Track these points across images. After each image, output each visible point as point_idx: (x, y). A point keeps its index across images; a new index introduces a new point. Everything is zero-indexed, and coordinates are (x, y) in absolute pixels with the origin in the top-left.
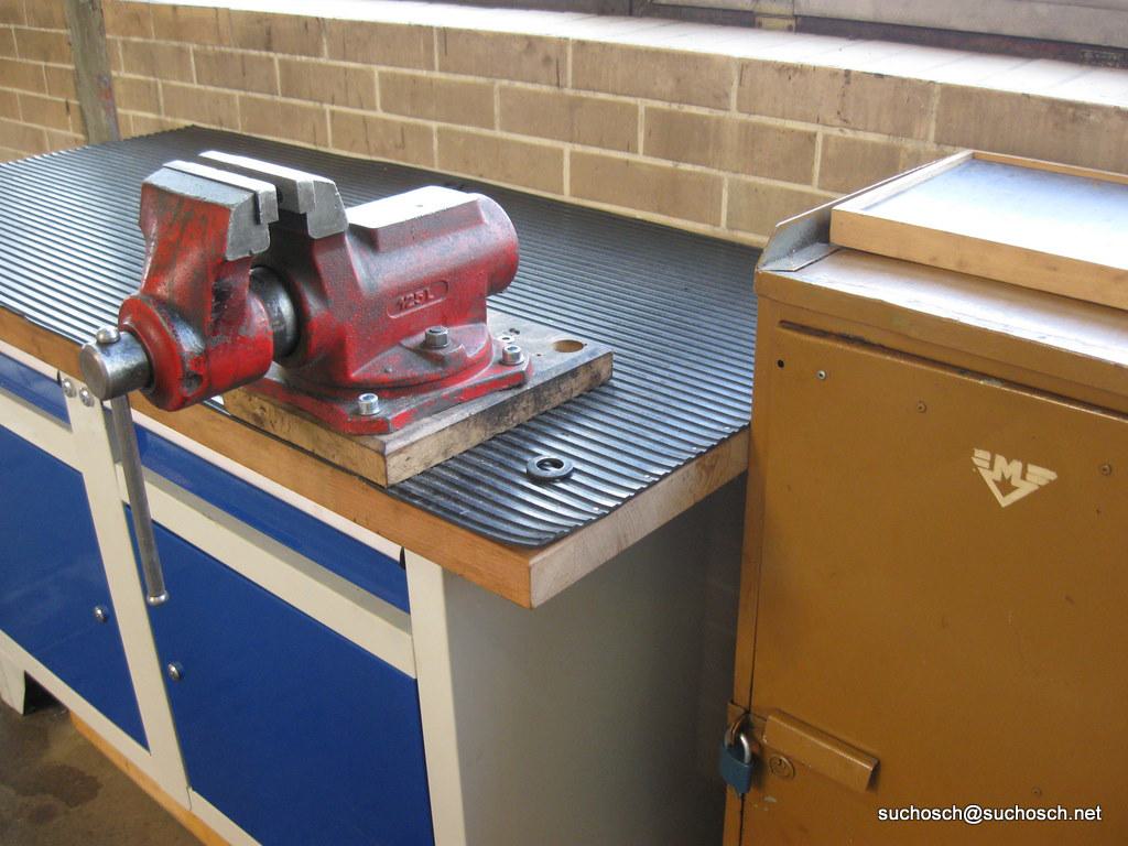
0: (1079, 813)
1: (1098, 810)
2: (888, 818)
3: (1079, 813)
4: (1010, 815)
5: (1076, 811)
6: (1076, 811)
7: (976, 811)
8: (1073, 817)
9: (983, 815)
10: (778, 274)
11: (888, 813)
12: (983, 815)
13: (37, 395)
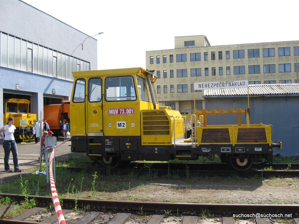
0: (286, 215)
1: (291, 214)
2: (235, 217)
3: (286, 215)
4: (240, 216)
5: (285, 215)
6: (285, 215)
7: (259, 215)
8: (284, 216)
9: (261, 216)
10: (173, 136)
11: (235, 215)
12: (261, 216)
13: (121, 211)
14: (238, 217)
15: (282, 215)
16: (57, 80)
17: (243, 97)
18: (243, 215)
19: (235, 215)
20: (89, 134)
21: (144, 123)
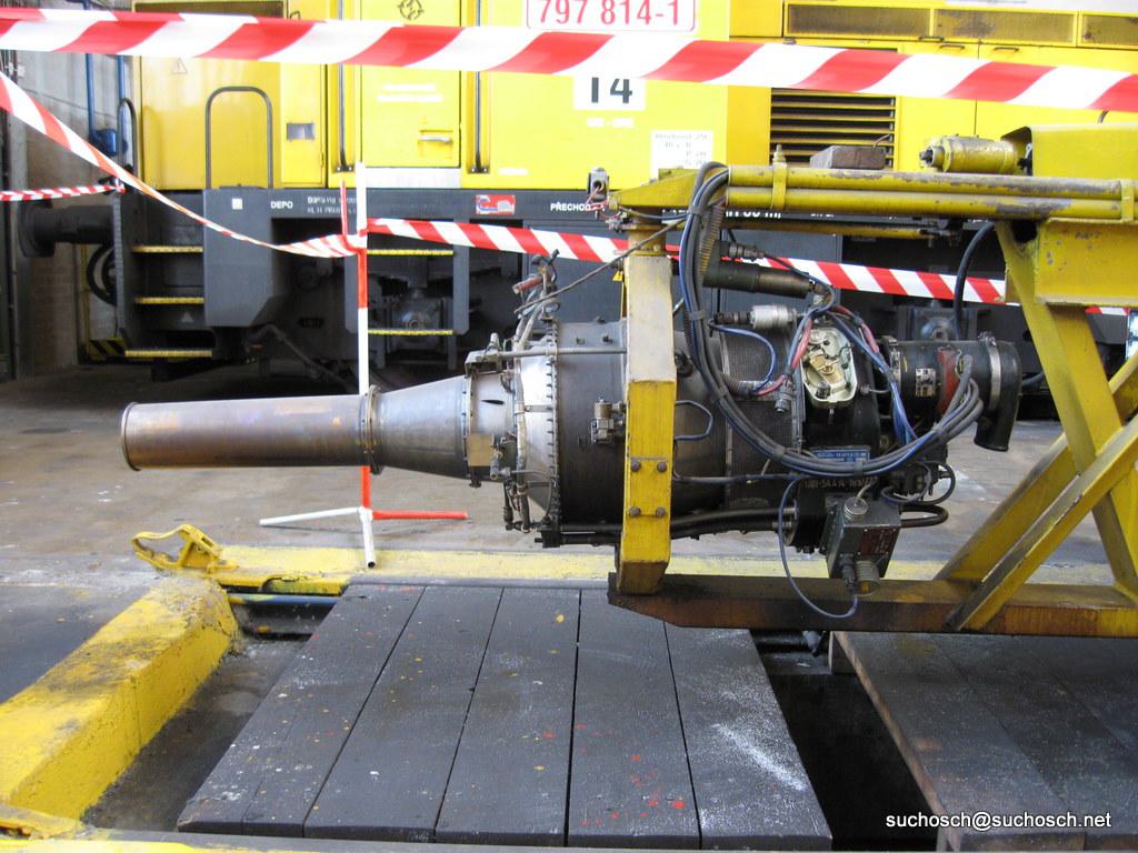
0: (1089, 820)
1: (1108, 817)
2: (896, 825)
3: (1089, 820)
4: (1019, 821)
5: (1086, 818)
6: (1086, 818)
7: (984, 818)
9: (992, 822)
11: (895, 820)
12: (992, 822)
14: (1010, 825)
15: (1072, 820)
16: (477, 580)
17: (535, 845)
18: (923, 820)
19: (895, 820)
20: (435, 273)
21: (774, 110)
